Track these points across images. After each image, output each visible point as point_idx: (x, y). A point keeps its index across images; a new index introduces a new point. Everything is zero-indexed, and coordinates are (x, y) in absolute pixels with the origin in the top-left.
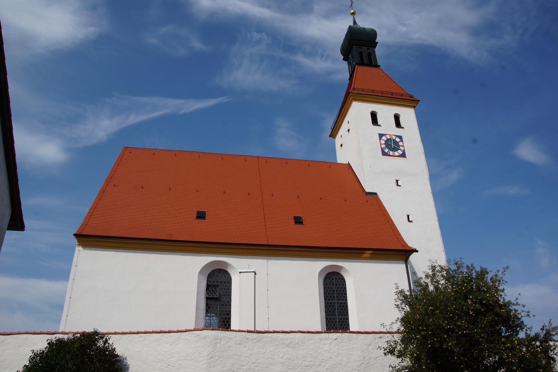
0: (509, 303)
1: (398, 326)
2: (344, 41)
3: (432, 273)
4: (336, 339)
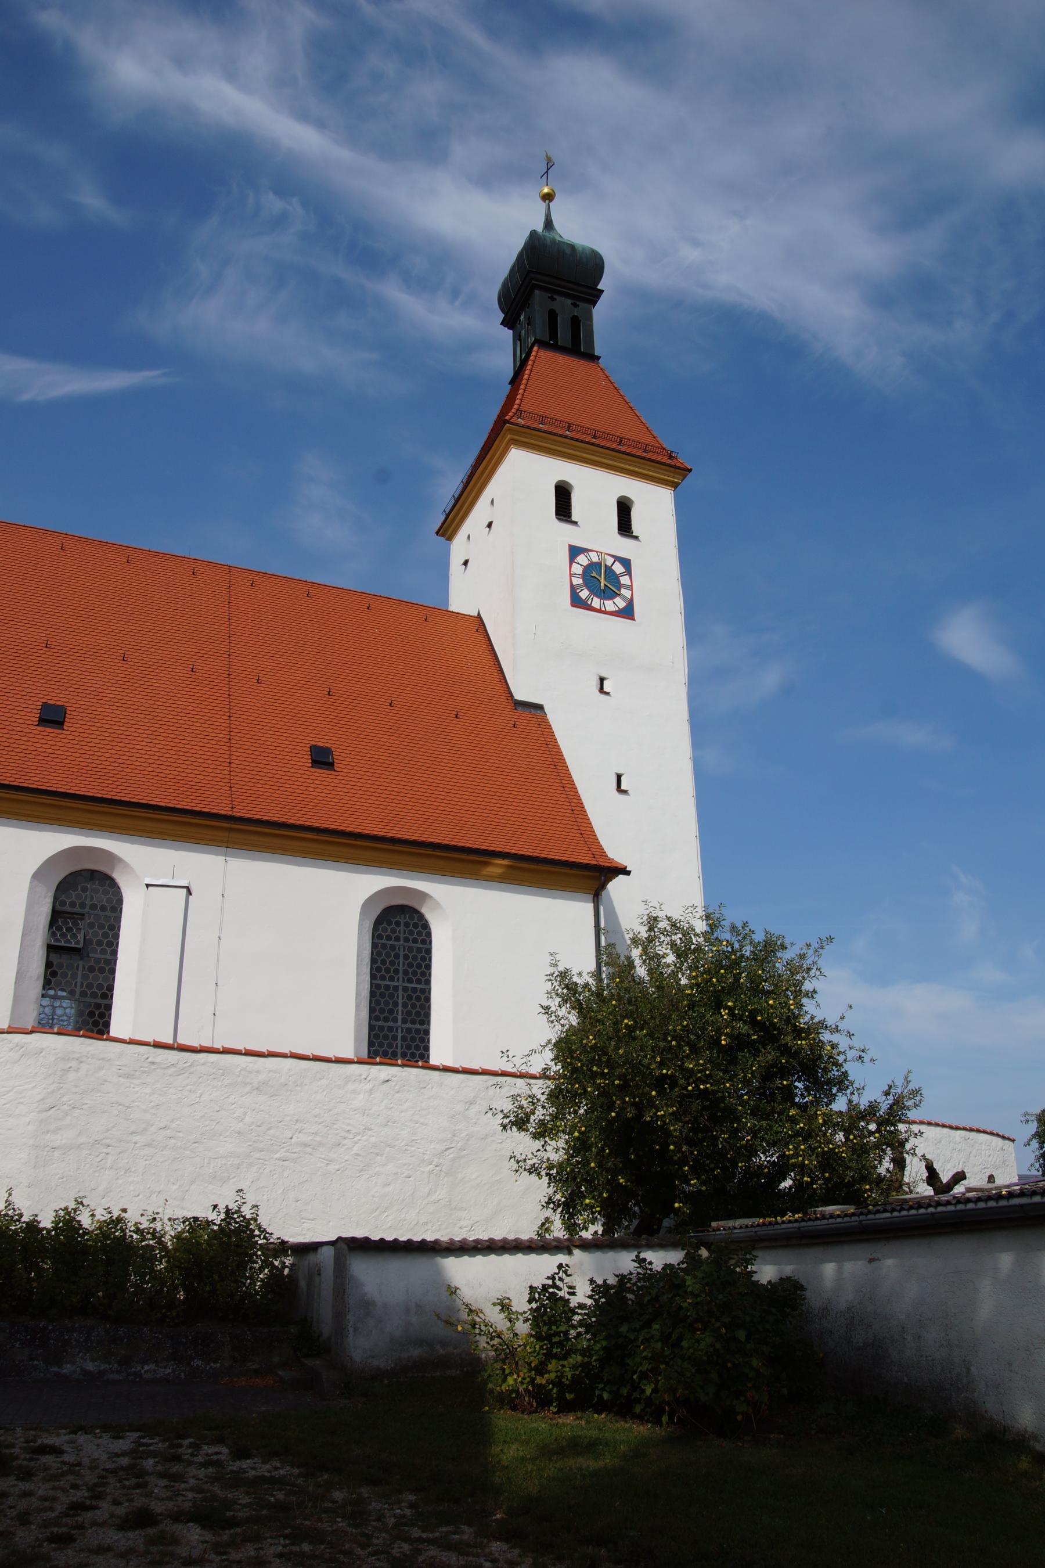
0: (822, 1025)
1: (544, 1060)
2: (512, 271)
3: (647, 936)
4: (388, 1081)
